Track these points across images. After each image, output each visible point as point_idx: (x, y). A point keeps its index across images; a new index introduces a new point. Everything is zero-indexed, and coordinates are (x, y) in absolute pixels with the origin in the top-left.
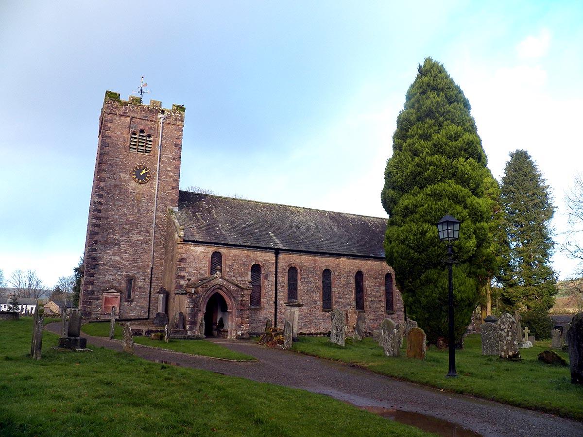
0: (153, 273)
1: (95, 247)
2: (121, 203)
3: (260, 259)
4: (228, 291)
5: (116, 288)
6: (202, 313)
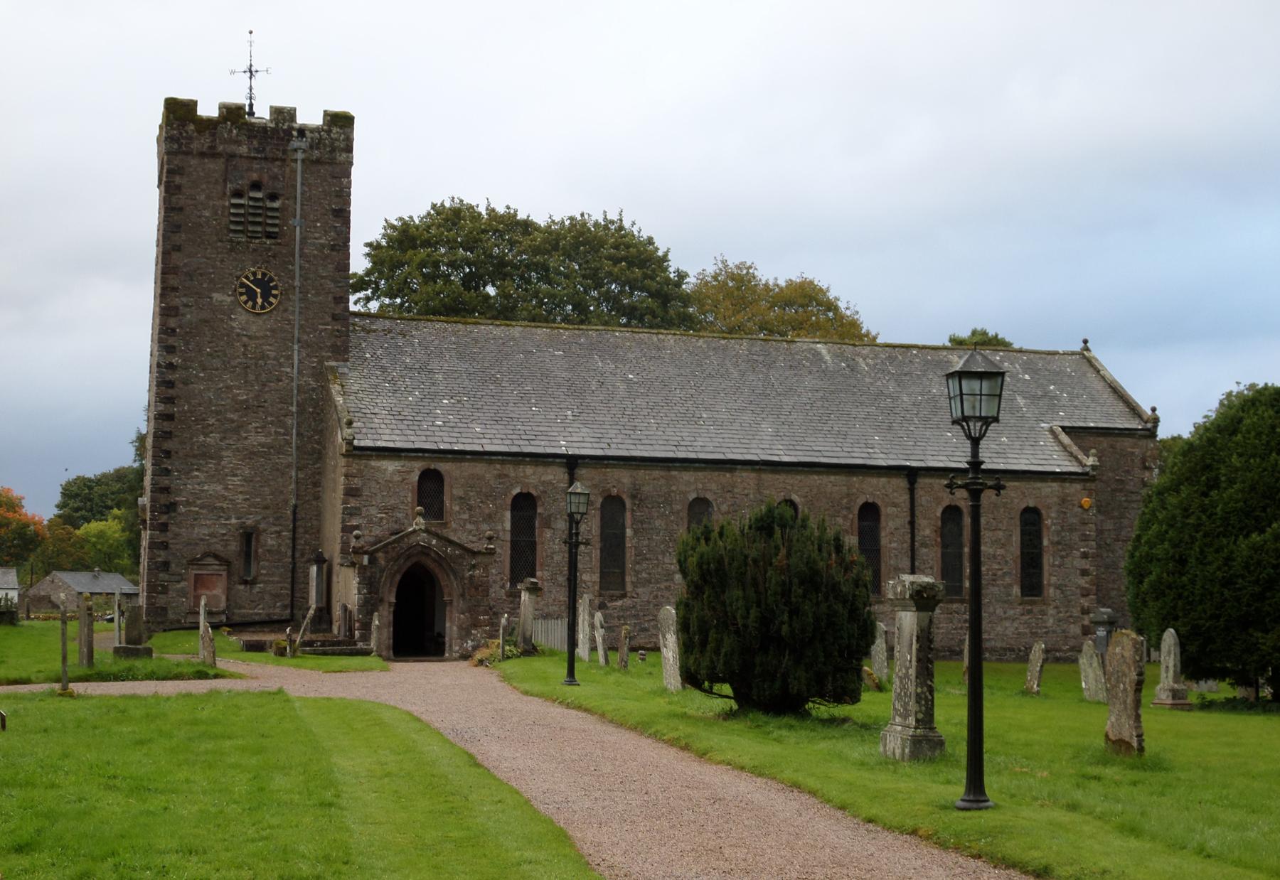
0: (299, 516)
1: (167, 445)
2: (217, 363)
3: (533, 480)
4: (440, 560)
5: (216, 556)
6: (386, 606)
